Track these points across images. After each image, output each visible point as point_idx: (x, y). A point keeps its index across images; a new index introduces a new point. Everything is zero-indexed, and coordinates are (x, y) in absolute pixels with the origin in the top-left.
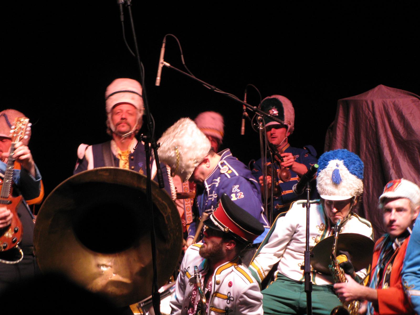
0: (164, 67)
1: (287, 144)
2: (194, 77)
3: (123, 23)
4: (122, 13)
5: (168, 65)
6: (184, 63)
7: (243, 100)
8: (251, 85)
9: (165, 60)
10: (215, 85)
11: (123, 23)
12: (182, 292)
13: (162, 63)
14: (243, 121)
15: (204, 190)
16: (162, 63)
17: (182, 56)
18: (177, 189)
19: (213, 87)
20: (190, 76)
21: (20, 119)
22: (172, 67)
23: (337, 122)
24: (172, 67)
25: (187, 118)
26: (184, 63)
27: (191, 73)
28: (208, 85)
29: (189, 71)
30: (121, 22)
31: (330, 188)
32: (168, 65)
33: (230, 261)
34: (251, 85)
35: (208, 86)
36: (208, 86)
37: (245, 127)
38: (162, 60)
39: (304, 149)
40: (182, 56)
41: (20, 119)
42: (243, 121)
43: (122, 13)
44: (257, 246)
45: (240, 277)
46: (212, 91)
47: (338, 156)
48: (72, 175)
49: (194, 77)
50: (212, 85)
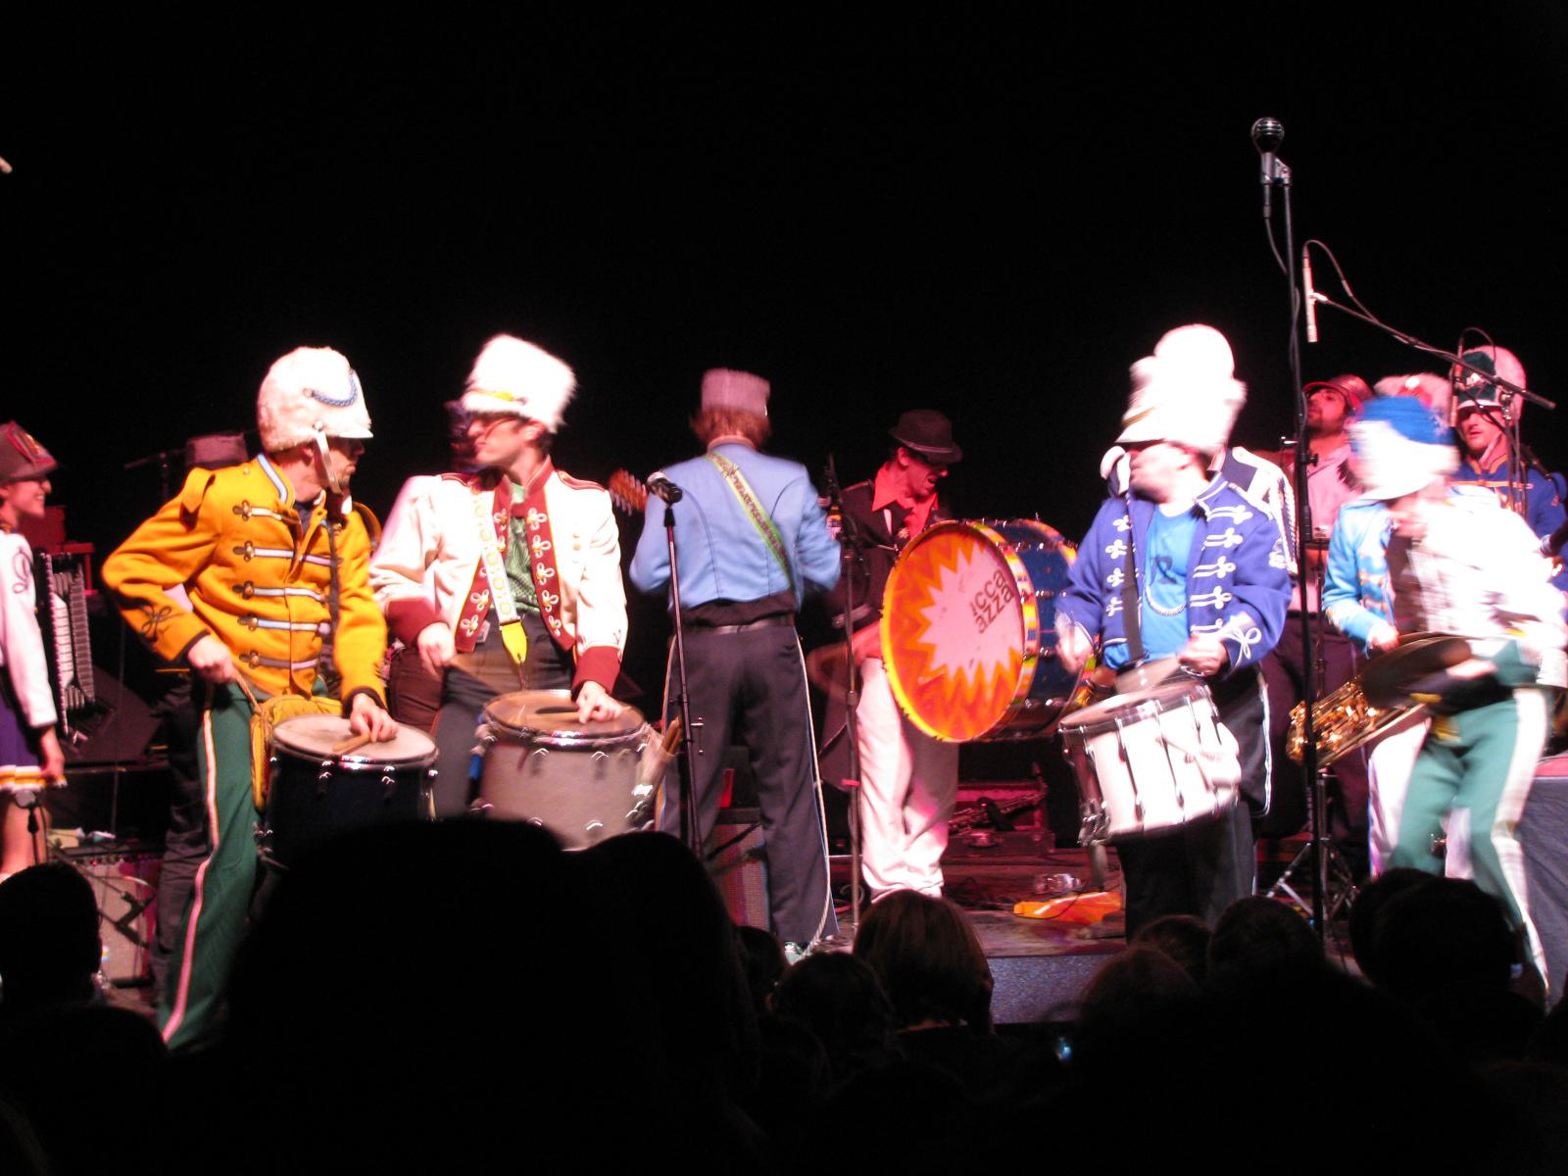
0: (1318, 305)
1: (719, 459)
2: (1374, 321)
3: (1267, 222)
4: (1267, 203)
5: (1323, 298)
6: (1351, 294)
8: (1478, 330)
9: (1317, 288)
11: (1267, 222)
13: (1312, 296)
16: (1312, 297)
17: (1344, 283)
19: (1412, 340)
20: (1364, 317)
21: (433, 672)
22: (1331, 302)
24: (1331, 302)
26: (1351, 294)
27: (1366, 311)
28: (1403, 335)
30: (1263, 219)
31: (1384, 581)
32: (1323, 298)
33: (1167, 704)
34: (1478, 330)
35: (1401, 338)
36: (1401, 338)
38: (1309, 291)
40: (1344, 283)
41: (433, 672)
43: (1267, 203)
45: (1201, 772)
46: (1409, 348)
48: (1497, 906)
49: (1374, 321)
50: (1409, 335)
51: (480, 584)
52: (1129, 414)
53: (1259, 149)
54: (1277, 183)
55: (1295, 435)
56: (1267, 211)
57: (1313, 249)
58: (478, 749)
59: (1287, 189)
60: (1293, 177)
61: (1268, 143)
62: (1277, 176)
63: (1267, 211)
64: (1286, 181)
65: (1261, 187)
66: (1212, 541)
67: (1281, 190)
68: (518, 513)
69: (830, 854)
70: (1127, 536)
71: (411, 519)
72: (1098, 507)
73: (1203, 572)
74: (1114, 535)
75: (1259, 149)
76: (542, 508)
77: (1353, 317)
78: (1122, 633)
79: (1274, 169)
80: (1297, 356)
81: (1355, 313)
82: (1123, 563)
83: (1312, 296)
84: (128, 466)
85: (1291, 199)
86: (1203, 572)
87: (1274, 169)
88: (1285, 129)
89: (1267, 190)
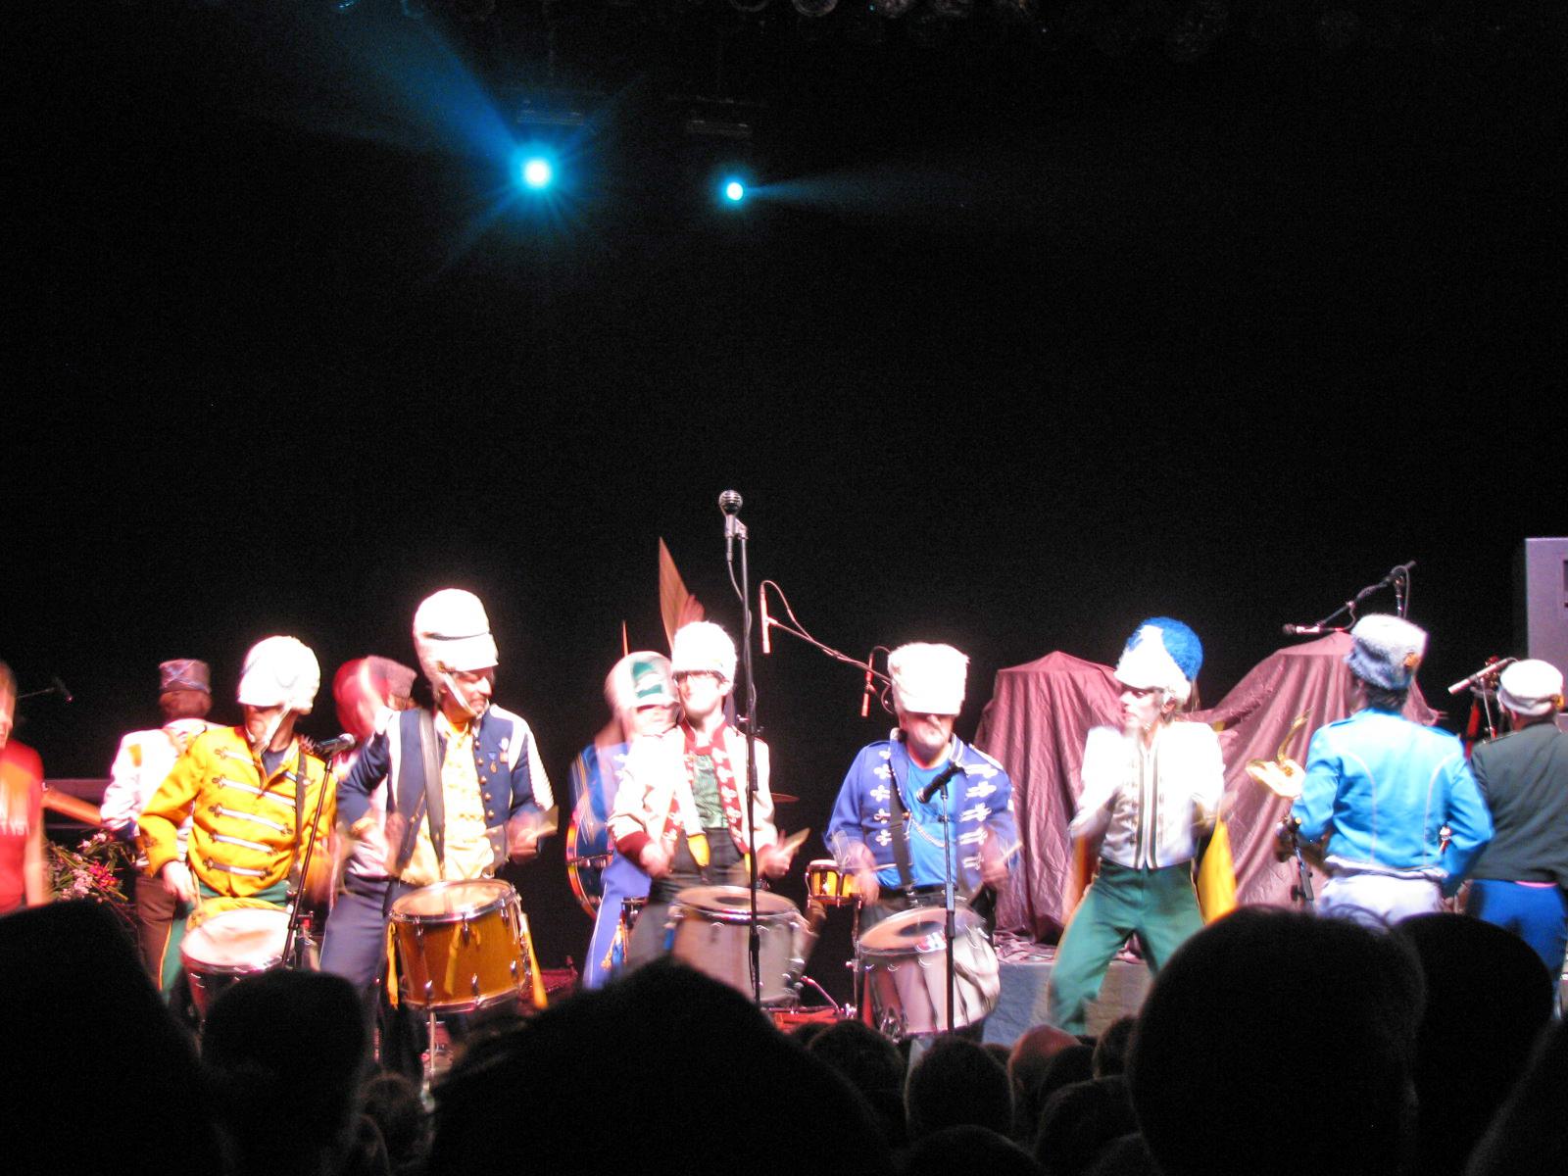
2: (810, 639)
3: (730, 563)
6: (793, 619)
7: (867, 663)
9: (770, 615)
10: (838, 650)
11: (730, 563)
12: (1372, 649)
13: (767, 621)
14: (866, 697)
15: (1493, 667)
18: (460, 741)
19: (836, 653)
23: (996, 704)
25: (498, 661)
26: (793, 619)
27: (804, 631)
29: (804, 631)
30: (727, 562)
32: (775, 622)
35: (829, 651)
36: (829, 651)
37: (869, 705)
39: (591, 864)
42: (866, 697)
44: (990, 710)
46: (834, 659)
47: (1008, 945)
49: (810, 639)
51: (674, 807)
52: (1089, 703)
53: (724, 513)
54: (736, 539)
55: (747, 714)
56: (729, 556)
57: (769, 589)
58: (670, 925)
59: (743, 541)
60: (749, 533)
61: (730, 508)
62: (737, 532)
63: (729, 556)
64: (743, 536)
65: (725, 541)
66: (972, 792)
67: (740, 542)
68: (705, 752)
69: (1091, 1051)
70: (889, 783)
71: (1464, 802)
72: (229, 725)
73: (967, 816)
74: (876, 782)
75: (724, 513)
76: (722, 747)
77: (792, 635)
78: (892, 858)
79: (735, 527)
80: (749, 659)
81: (796, 633)
82: (888, 804)
83: (767, 621)
84: (865, 713)
85: (748, 548)
86: (967, 816)
87: (735, 527)
88: (744, 499)
89: (730, 542)
